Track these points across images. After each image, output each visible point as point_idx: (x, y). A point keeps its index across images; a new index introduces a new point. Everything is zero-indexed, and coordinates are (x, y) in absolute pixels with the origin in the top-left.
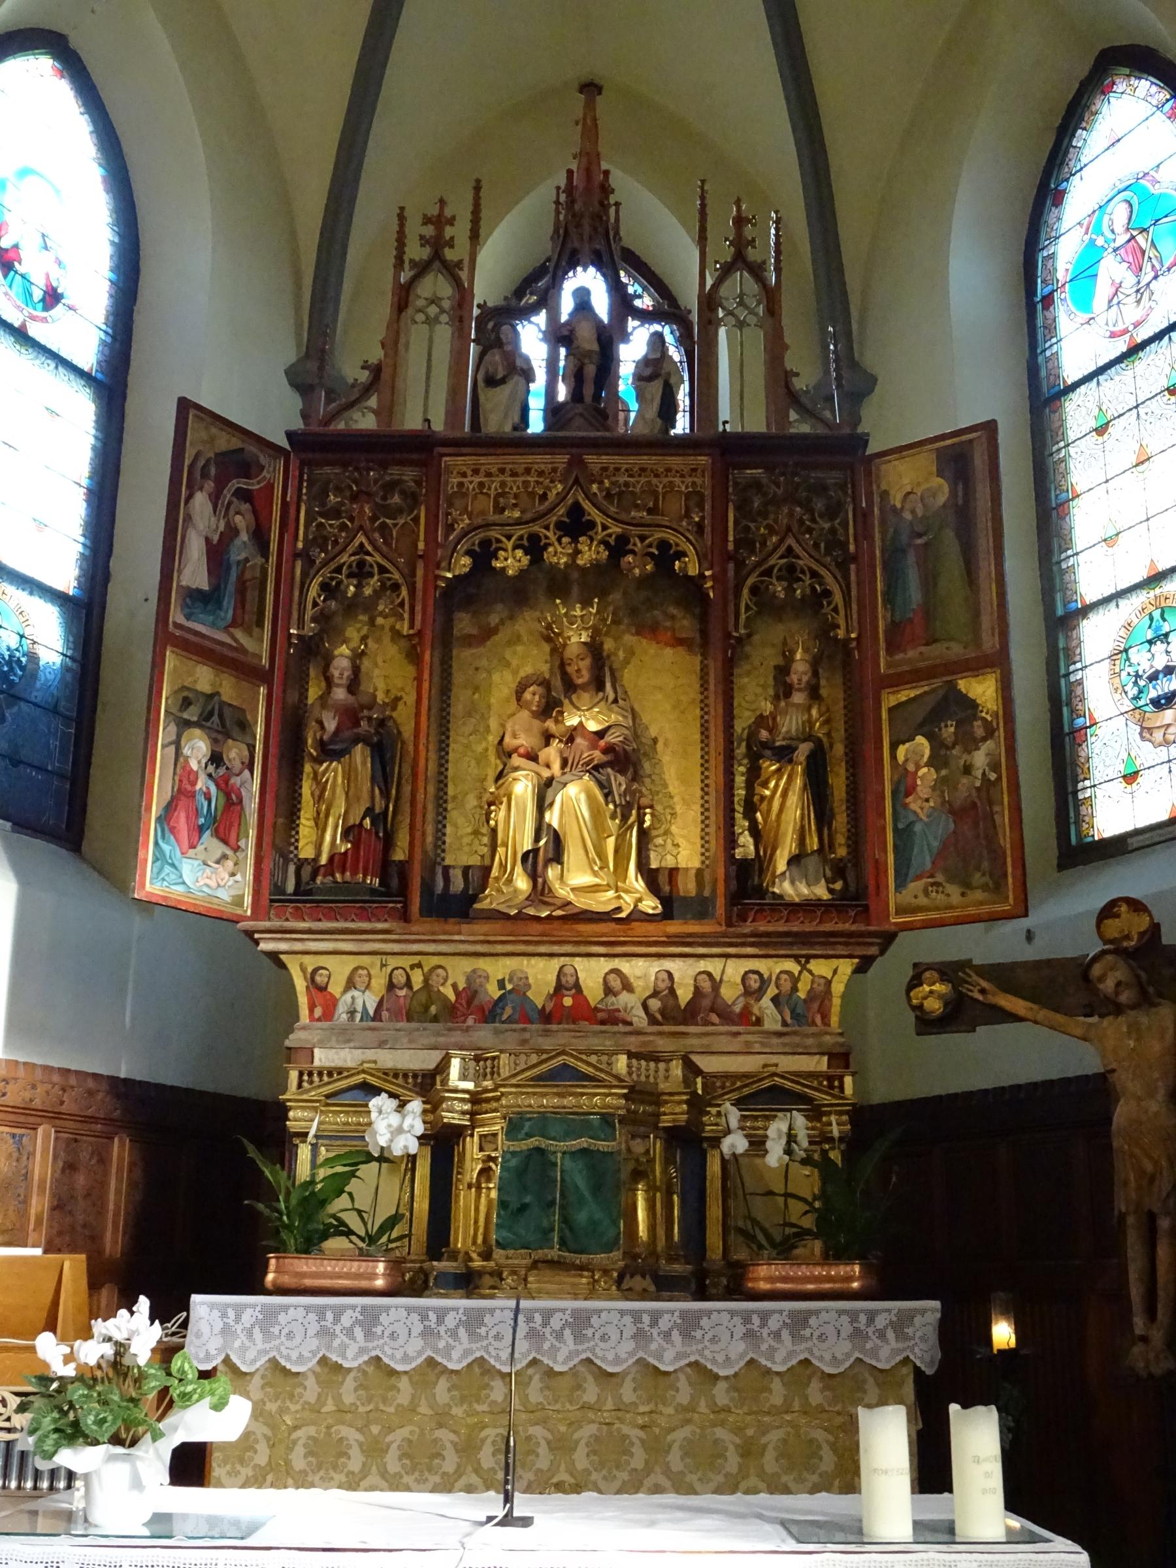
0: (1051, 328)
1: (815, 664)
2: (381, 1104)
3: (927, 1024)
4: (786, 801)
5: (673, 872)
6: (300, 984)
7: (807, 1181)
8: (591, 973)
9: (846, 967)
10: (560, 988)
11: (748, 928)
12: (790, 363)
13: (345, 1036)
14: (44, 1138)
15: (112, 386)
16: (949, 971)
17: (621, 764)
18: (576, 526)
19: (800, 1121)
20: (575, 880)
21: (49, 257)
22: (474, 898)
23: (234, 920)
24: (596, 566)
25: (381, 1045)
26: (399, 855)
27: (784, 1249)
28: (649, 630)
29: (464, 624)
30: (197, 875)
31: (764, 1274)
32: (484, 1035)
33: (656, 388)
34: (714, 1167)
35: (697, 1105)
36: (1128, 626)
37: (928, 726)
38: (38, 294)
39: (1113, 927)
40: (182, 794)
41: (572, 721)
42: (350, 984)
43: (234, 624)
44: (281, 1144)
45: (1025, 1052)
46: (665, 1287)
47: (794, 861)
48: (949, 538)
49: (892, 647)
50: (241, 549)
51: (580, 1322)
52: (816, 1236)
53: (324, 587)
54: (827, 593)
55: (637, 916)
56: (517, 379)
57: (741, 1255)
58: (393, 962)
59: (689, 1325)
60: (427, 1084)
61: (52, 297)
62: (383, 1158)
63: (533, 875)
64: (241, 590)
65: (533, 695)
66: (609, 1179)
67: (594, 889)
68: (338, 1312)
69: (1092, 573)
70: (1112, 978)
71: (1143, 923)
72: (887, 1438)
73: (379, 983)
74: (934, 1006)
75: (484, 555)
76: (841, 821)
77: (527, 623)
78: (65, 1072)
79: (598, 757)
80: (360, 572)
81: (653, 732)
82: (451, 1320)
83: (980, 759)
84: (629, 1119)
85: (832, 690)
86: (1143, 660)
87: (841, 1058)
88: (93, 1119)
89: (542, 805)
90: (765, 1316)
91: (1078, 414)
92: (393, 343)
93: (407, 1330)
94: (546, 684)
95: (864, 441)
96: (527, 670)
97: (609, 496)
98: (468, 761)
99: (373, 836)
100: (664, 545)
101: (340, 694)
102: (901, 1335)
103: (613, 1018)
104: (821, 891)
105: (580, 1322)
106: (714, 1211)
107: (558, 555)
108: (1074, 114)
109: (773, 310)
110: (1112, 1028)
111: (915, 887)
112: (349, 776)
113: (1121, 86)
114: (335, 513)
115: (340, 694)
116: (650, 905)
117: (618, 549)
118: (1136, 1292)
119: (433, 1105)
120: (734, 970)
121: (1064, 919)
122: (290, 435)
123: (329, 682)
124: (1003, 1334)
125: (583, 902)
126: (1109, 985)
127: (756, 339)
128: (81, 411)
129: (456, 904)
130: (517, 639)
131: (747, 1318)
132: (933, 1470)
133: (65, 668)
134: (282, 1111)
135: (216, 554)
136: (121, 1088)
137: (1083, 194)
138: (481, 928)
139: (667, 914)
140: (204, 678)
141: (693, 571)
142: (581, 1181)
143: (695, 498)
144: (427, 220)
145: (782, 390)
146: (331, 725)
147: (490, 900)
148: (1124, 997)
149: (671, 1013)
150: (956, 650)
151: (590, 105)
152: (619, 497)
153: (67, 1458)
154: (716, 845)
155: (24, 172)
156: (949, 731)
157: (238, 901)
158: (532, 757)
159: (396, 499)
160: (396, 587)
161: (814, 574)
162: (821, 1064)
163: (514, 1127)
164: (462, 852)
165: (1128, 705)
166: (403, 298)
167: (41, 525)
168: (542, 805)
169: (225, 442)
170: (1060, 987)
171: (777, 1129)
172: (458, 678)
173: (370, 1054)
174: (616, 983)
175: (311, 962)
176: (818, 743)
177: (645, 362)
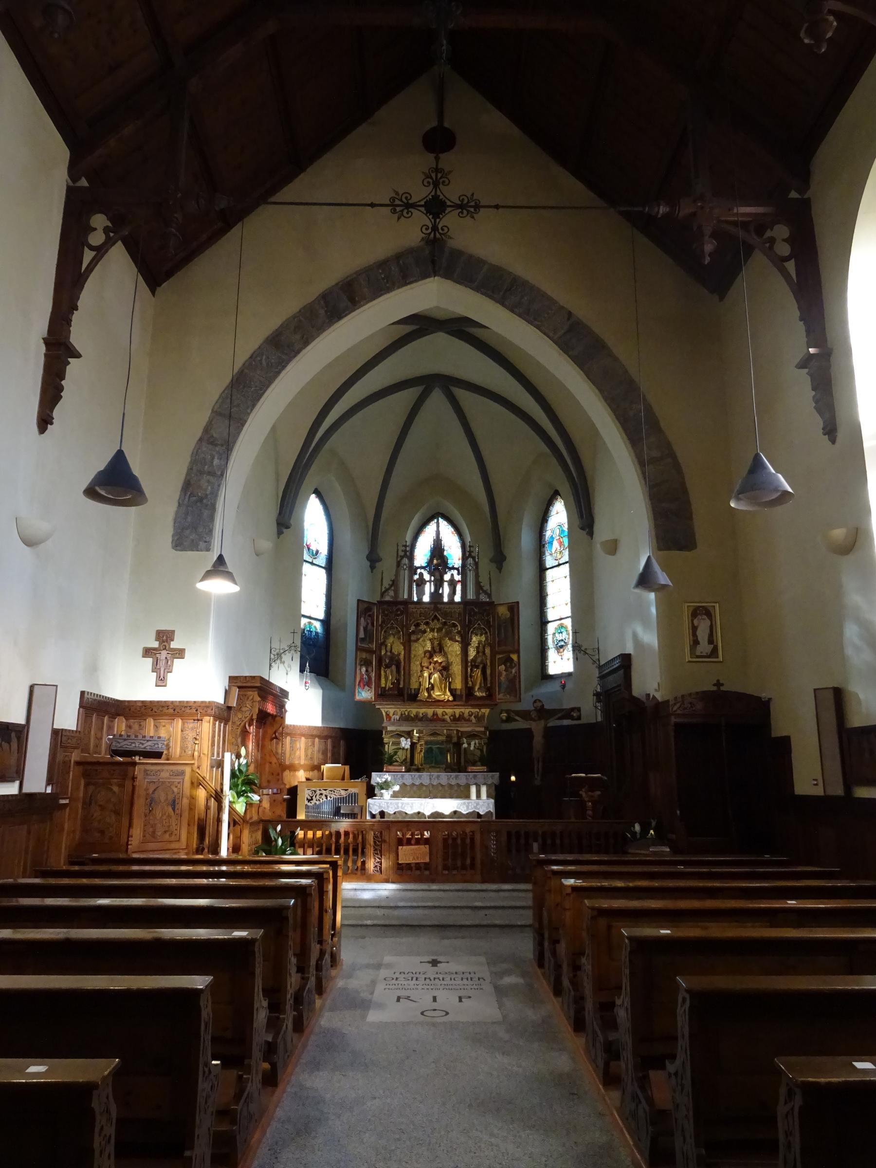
0: (544, 554)
2: (402, 739)
3: (503, 721)
4: (478, 673)
7: (478, 753)
8: (440, 711)
11: (470, 703)
12: (480, 579)
13: (393, 724)
14: (329, 741)
15: (329, 568)
16: (507, 711)
17: (445, 669)
20: (436, 694)
26: (401, 686)
30: (365, 695)
31: (470, 769)
32: (419, 724)
35: (459, 738)
44: (383, 744)
45: (520, 724)
46: (453, 771)
49: (499, 645)
50: (370, 626)
51: (438, 777)
55: (448, 701)
59: (457, 777)
60: (409, 734)
62: (403, 749)
65: (428, 655)
66: (443, 752)
70: (534, 714)
72: (473, 789)
73: (399, 713)
74: (504, 718)
83: (514, 671)
91: (549, 574)
93: (409, 778)
98: (415, 667)
99: (396, 684)
101: (389, 654)
103: (444, 720)
104: (484, 694)
105: (438, 777)
107: (432, 624)
108: (550, 503)
109: (477, 568)
114: (386, 615)
116: (451, 698)
124: (513, 778)
125: (438, 698)
128: (322, 573)
129: (413, 697)
134: (383, 739)
135: (365, 629)
136: (341, 729)
139: (454, 700)
140: (364, 655)
143: (460, 614)
147: (420, 697)
149: (456, 719)
156: (509, 664)
163: (427, 743)
164: (414, 685)
166: (399, 564)
168: (430, 678)
169: (366, 606)
170: (525, 715)
172: (412, 648)
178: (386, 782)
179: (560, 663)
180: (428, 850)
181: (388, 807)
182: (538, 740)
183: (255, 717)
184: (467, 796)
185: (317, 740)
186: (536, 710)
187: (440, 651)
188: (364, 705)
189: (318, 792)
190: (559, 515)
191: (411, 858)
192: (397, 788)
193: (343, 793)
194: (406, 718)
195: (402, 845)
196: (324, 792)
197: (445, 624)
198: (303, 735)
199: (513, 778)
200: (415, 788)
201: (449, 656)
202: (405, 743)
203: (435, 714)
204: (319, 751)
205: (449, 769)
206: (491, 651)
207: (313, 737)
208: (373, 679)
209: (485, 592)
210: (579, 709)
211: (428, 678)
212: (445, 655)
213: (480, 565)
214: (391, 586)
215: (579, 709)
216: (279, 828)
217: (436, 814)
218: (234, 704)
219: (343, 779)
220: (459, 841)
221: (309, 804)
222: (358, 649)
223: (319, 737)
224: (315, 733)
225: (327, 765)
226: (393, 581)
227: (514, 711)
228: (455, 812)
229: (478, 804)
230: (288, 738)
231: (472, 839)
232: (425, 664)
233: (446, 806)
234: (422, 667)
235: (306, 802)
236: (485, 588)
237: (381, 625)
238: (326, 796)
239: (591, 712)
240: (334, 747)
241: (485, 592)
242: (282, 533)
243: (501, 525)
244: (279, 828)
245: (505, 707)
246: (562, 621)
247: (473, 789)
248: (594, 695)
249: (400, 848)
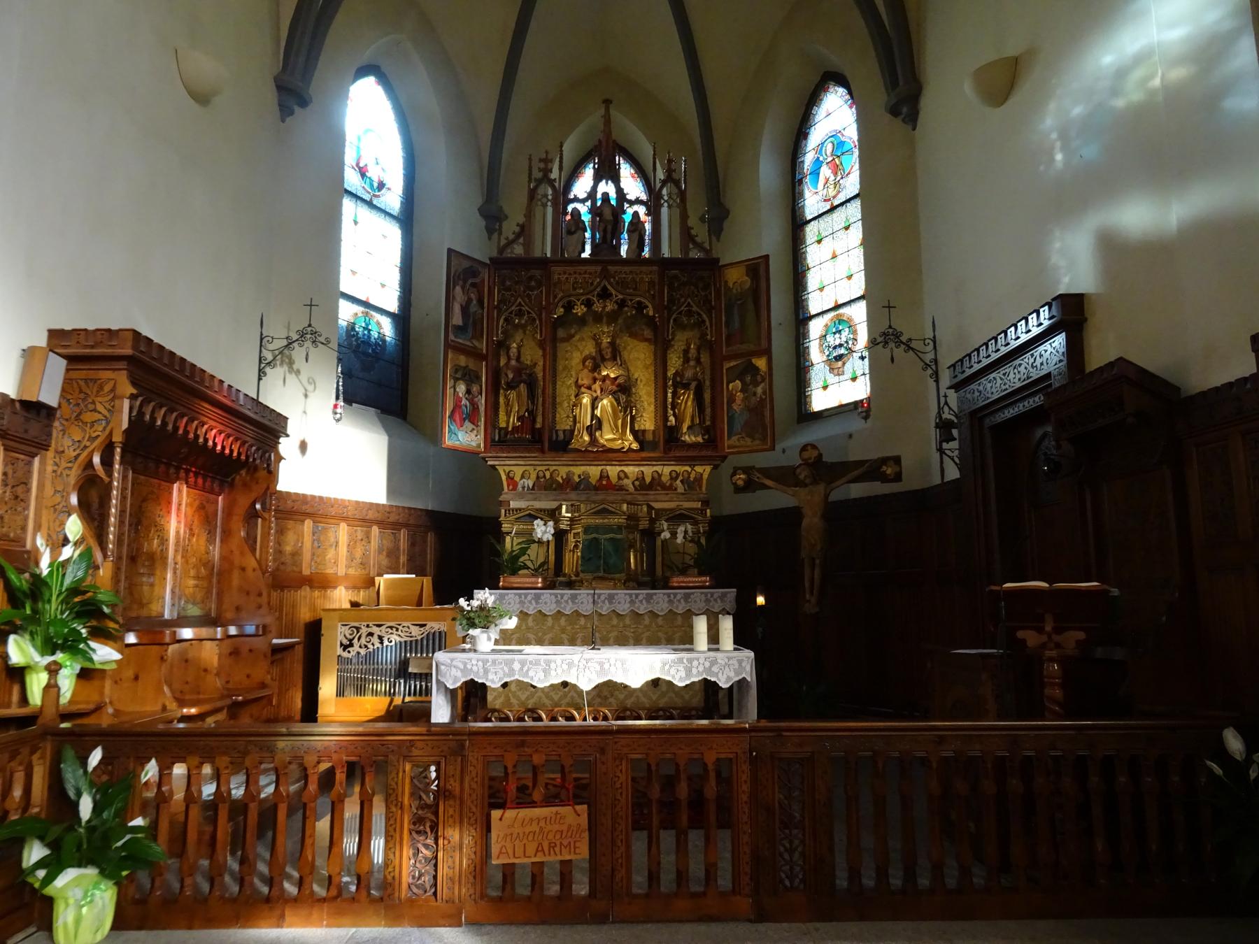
0: (801, 195)
1: (698, 350)
3: (738, 490)
4: (687, 402)
5: (644, 431)
6: (504, 477)
7: (692, 549)
8: (613, 471)
9: (708, 469)
10: (601, 477)
11: (672, 454)
13: (521, 496)
14: (403, 534)
15: (407, 219)
16: (746, 470)
17: (623, 391)
18: (605, 295)
19: (689, 527)
20: (607, 436)
21: (379, 168)
22: (569, 442)
23: (478, 453)
24: (613, 311)
25: (535, 499)
26: (538, 426)
27: (684, 571)
28: (633, 335)
29: (561, 333)
30: (464, 437)
31: (675, 581)
32: (573, 495)
33: (636, 236)
34: (659, 543)
36: (826, 325)
37: (741, 377)
38: (376, 185)
39: (806, 455)
40: (457, 406)
41: (604, 373)
42: (523, 477)
43: (473, 338)
44: (500, 536)
45: (775, 498)
46: (641, 585)
47: (689, 428)
48: (750, 306)
49: (728, 345)
50: (474, 307)
51: (611, 598)
53: (506, 320)
54: (704, 321)
55: (630, 450)
56: (580, 232)
57: (668, 574)
58: (539, 468)
60: (553, 515)
61: (381, 186)
62: (540, 542)
63: (591, 435)
64: (475, 324)
66: (621, 549)
67: (614, 440)
68: (526, 595)
69: (815, 303)
70: (803, 474)
71: (815, 453)
72: (701, 626)
73: (534, 476)
74: (740, 483)
75: (569, 307)
76: (708, 411)
77: (588, 331)
78: (410, 509)
79: (614, 388)
80: (520, 314)
81: (636, 376)
82: (565, 598)
83: (759, 390)
84: (628, 527)
85: (705, 358)
86: (832, 340)
87: (706, 503)
88: (420, 526)
89: (594, 407)
90: (675, 595)
91: (811, 232)
92: (529, 214)
93: (549, 601)
94: (594, 358)
95: (718, 260)
96: (587, 352)
97: (618, 283)
98: (565, 389)
99: (528, 420)
100: (639, 303)
101: (513, 363)
102: (722, 601)
103: (621, 488)
104: (700, 439)
106: (659, 559)
107: (597, 307)
108: (813, 99)
110: (803, 492)
111: (735, 438)
112: (519, 396)
113: (831, 90)
114: (508, 289)
115: (513, 363)
116: (635, 446)
117: (622, 304)
118: (807, 585)
119: (557, 522)
120: (666, 470)
121: (789, 448)
122: (491, 259)
123: (509, 358)
124: (761, 600)
125: (609, 445)
126: (802, 477)
127: (677, 211)
128: (394, 233)
129: (561, 445)
130: (582, 339)
131: (669, 595)
132: (714, 638)
133: (396, 345)
134: (500, 524)
135: (465, 310)
136: (430, 514)
137: (816, 136)
138: (571, 455)
139: (642, 449)
140: (463, 360)
141: (651, 313)
142: (610, 548)
143: (651, 283)
144: (541, 160)
145: (687, 236)
146: (511, 376)
147: (574, 444)
148: (807, 481)
149: (643, 486)
150: (752, 347)
151: (607, 109)
152: (622, 285)
153: (471, 632)
154: (660, 423)
155: (367, 131)
156: (748, 379)
157: (479, 446)
158: (589, 388)
159: (533, 283)
160: (534, 320)
161: (699, 314)
162: (699, 505)
163: (587, 530)
164: (563, 424)
165: (825, 358)
166: (532, 194)
167: (383, 286)
168: (594, 407)
169: (466, 264)
170: (785, 476)
171: (681, 529)
172: (559, 354)
173: (531, 503)
174: (622, 475)
175: (507, 469)
176: (699, 381)
177: (631, 223)
178: (482, 608)
179: (837, 387)
180: (584, 820)
181: (486, 672)
182: (812, 521)
183: (118, 438)
184: (684, 640)
185: (375, 530)
186: (806, 463)
187: (614, 358)
188: (464, 456)
189: (364, 631)
190: (836, 116)
191: (531, 849)
192: (511, 623)
193: (416, 631)
194: (547, 486)
195: (502, 806)
196: (375, 630)
197: (622, 304)
198: (345, 519)
199: (761, 600)
200: (563, 621)
201: (632, 369)
202: (543, 530)
203: (604, 476)
204: (380, 551)
205: (634, 581)
206: (712, 356)
207: (366, 522)
208: (482, 409)
209: (699, 246)
210: (897, 460)
211: (590, 409)
212: (623, 364)
213: (689, 195)
214: (518, 236)
215: (897, 460)
216: (96, 757)
217: (608, 690)
218: (50, 396)
219: (419, 603)
220: (683, 790)
221: (345, 654)
222: (448, 345)
223: (381, 524)
224: (371, 515)
225: (386, 576)
226: (522, 227)
227: (761, 471)
228: (656, 683)
229: (714, 662)
230: (308, 524)
231: (725, 781)
232: (585, 381)
233: (636, 666)
234: (579, 387)
235: (339, 651)
236: (698, 239)
237: (497, 307)
238: (381, 638)
239: (933, 463)
240: (412, 544)
241: (699, 246)
242: (292, 113)
243: (720, 146)
244: (96, 757)
245: (746, 460)
246: (841, 311)
247: (701, 626)
248: (937, 426)
249: (496, 814)
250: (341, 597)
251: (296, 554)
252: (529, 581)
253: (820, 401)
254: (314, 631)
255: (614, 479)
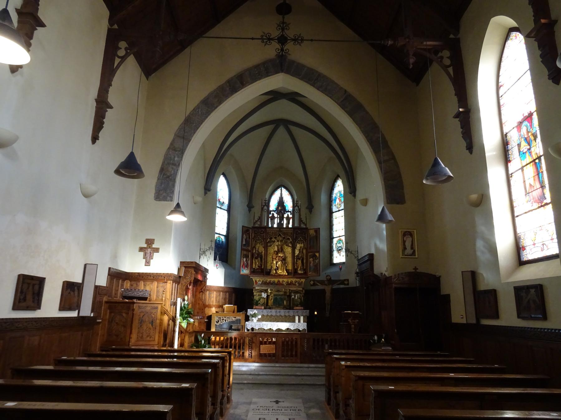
3: (311, 285)
4: (300, 262)
7: (299, 300)
8: (281, 280)
13: (258, 286)
14: (227, 294)
16: (314, 281)
17: (284, 260)
20: (280, 272)
27: (297, 306)
30: (245, 271)
31: (295, 308)
32: (271, 286)
35: (290, 293)
40: (244, 264)
45: (320, 287)
46: (287, 309)
50: (248, 239)
51: (280, 312)
52: (247, 311)
60: (266, 291)
66: (282, 300)
70: (326, 283)
72: (297, 318)
87: (303, 289)
91: (334, 214)
93: (265, 312)
98: (269, 258)
99: (260, 267)
103: (283, 284)
108: (335, 181)
116: (286, 274)
120: (294, 280)
124: (316, 313)
128: (226, 212)
129: (268, 273)
135: (246, 240)
136: (233, 288)
140: (245, 253)
147: (272, 273)
149: (289, 284)
163: (274, 295)
164: (269, 268)
166: (262, 209)
170: (322, 282)
179: (339, 258)
182: (328, 294)
183: (192, 281)
184: (294, 321)
187: (282, 251)
190: (339, 187)
192: (260, 317)
193: (234, 319)
198: (215, 291)
199: (316, 313)
202: (264, 295)
203: (279, 281)
205: (285, 308)
207: (219, 291)
209: (304, 223)
210: (348, 280)
211: (276, 264)
212: (284, 253)
215: (348, 280)
216: (203, 335)
217: (279, 330)
219: (234, 312)
220: (290, 343)
223: (222, 291)
224: (221, 290)
227: (317, 281)
230: (208, 292)
233: (284, 326)
239: (354, 281)
244: (203, 335)
247: (297, 318)
250: (214, 310)
251: (205, 299)
252: (260, 307)
253: (336, 261)
254: (210, 318)
255: (281, 282)
